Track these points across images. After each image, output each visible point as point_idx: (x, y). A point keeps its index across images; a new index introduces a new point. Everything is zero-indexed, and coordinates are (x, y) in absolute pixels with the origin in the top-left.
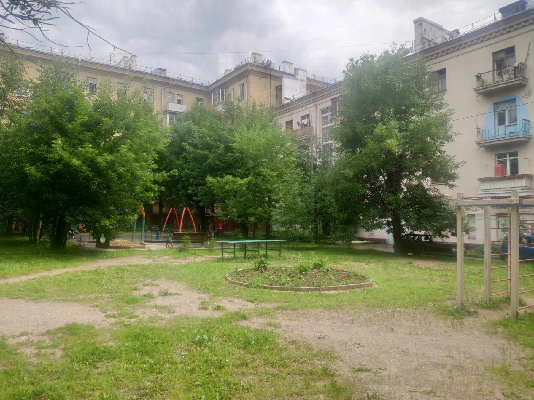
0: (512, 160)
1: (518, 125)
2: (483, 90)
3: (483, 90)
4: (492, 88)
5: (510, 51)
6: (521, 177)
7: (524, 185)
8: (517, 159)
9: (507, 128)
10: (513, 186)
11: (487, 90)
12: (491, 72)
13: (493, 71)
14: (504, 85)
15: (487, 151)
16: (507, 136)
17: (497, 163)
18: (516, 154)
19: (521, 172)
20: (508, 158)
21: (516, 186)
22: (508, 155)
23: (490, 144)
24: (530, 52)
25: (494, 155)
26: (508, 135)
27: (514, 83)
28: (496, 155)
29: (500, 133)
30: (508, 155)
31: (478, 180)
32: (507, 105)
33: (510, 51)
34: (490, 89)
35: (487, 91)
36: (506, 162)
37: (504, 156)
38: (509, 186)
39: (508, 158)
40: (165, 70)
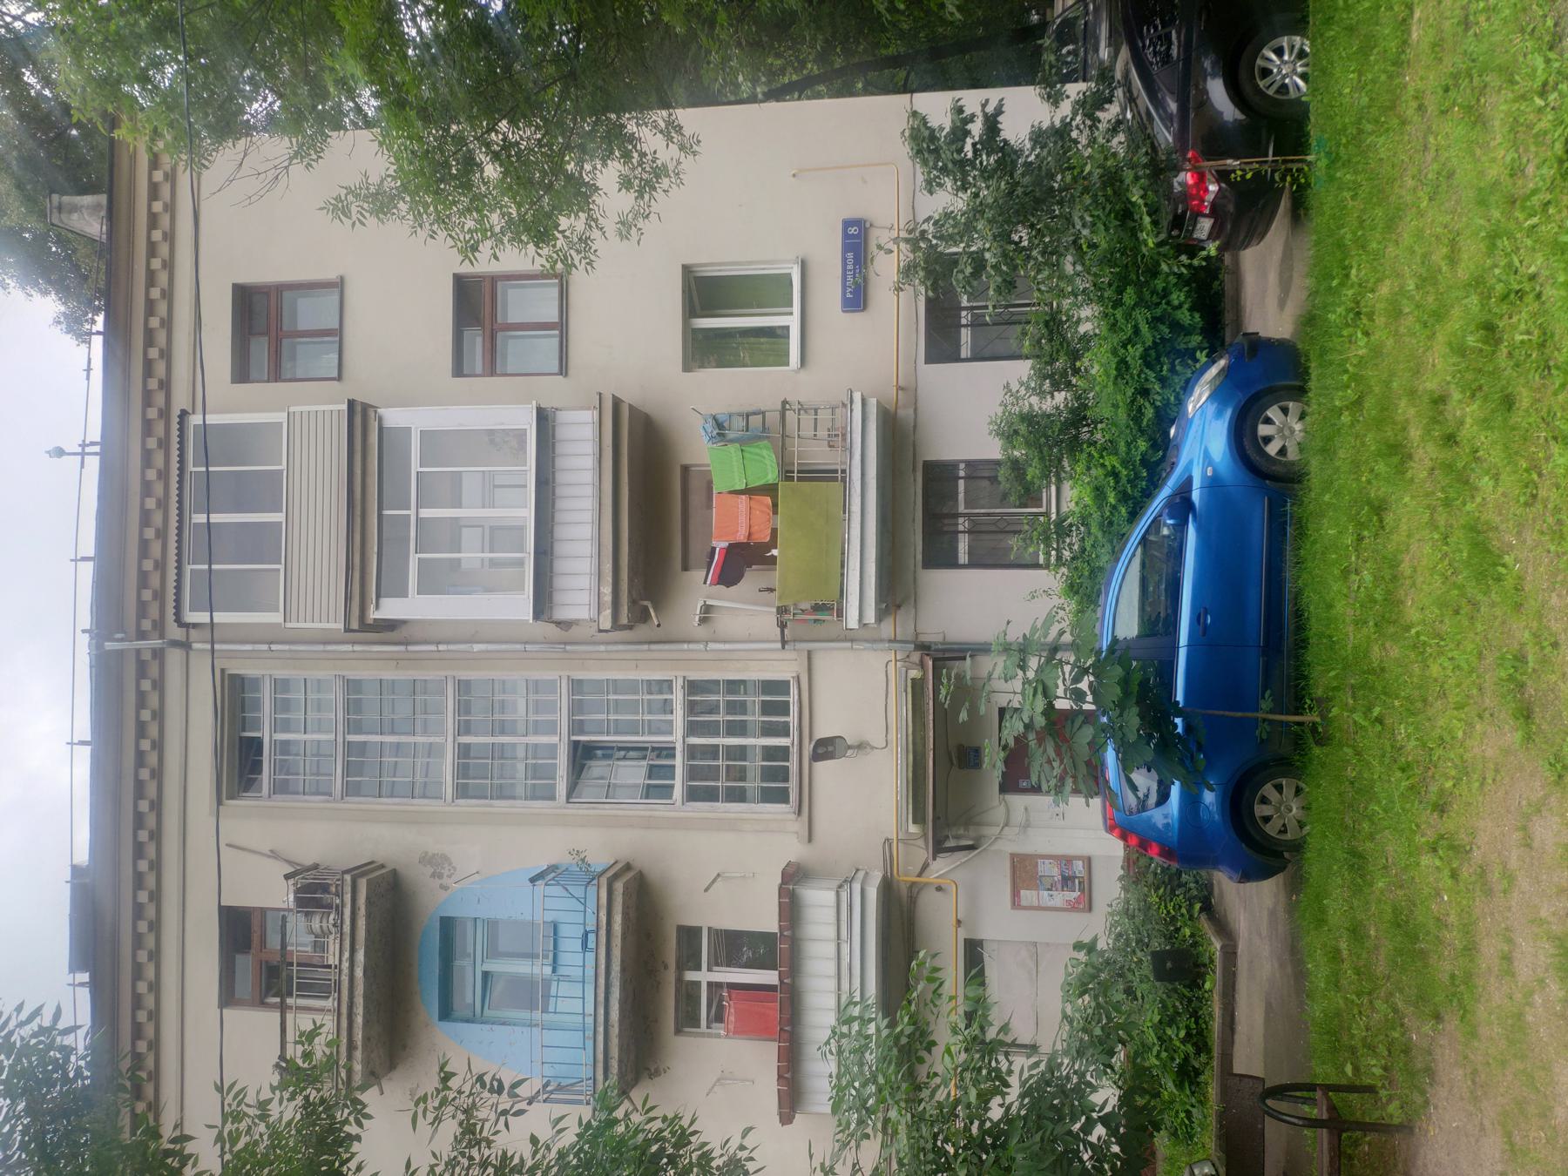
0: (715, 962)
1: (561, 917)
2: (358, 1054)
3: (358, 1054)
4: (359, 1010)
5: (239, 928)
6: (791, 909)
7: (829, 897)
8: (716, 934)
9: (562, 971)
10: (831, 949)
11: (359, 1036)
12: (289, 1016)
13: (283, 1009)
14: (360, 956)
15: (657, 1073)
16: (590, 972)
17: (719, 1029)
18: (689, 935)
19: (766, 920)
20: (703, 977)
21: (832, 933)
22: (691, 976)
23: (615, 1031)
24: (266, 850)
25: (681, 1041)
26: (590, 956)
27: (362, 911)
28: (678, 1031)
29: (577, 1006)
30: (691, 976)
31: (786, 1118)
32: (461, 963)
33: (239, 928)
34: (359, 1020)
35: (367, 1039)
36: (719, 985)
37: (688, 994)
38: (831, 968)
39: (703, 977)
40: (1090, 909)
